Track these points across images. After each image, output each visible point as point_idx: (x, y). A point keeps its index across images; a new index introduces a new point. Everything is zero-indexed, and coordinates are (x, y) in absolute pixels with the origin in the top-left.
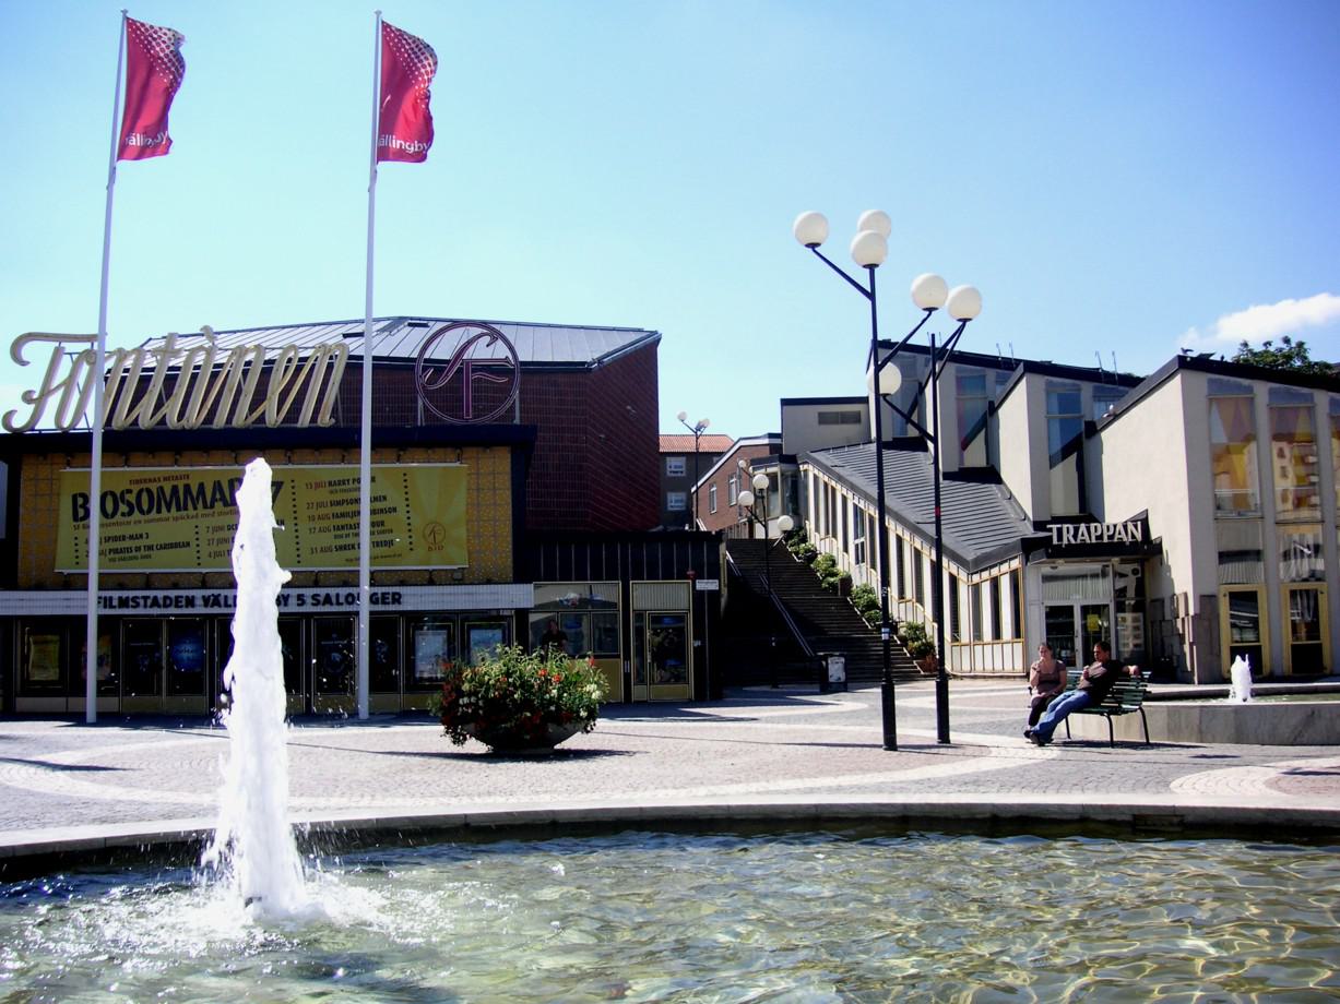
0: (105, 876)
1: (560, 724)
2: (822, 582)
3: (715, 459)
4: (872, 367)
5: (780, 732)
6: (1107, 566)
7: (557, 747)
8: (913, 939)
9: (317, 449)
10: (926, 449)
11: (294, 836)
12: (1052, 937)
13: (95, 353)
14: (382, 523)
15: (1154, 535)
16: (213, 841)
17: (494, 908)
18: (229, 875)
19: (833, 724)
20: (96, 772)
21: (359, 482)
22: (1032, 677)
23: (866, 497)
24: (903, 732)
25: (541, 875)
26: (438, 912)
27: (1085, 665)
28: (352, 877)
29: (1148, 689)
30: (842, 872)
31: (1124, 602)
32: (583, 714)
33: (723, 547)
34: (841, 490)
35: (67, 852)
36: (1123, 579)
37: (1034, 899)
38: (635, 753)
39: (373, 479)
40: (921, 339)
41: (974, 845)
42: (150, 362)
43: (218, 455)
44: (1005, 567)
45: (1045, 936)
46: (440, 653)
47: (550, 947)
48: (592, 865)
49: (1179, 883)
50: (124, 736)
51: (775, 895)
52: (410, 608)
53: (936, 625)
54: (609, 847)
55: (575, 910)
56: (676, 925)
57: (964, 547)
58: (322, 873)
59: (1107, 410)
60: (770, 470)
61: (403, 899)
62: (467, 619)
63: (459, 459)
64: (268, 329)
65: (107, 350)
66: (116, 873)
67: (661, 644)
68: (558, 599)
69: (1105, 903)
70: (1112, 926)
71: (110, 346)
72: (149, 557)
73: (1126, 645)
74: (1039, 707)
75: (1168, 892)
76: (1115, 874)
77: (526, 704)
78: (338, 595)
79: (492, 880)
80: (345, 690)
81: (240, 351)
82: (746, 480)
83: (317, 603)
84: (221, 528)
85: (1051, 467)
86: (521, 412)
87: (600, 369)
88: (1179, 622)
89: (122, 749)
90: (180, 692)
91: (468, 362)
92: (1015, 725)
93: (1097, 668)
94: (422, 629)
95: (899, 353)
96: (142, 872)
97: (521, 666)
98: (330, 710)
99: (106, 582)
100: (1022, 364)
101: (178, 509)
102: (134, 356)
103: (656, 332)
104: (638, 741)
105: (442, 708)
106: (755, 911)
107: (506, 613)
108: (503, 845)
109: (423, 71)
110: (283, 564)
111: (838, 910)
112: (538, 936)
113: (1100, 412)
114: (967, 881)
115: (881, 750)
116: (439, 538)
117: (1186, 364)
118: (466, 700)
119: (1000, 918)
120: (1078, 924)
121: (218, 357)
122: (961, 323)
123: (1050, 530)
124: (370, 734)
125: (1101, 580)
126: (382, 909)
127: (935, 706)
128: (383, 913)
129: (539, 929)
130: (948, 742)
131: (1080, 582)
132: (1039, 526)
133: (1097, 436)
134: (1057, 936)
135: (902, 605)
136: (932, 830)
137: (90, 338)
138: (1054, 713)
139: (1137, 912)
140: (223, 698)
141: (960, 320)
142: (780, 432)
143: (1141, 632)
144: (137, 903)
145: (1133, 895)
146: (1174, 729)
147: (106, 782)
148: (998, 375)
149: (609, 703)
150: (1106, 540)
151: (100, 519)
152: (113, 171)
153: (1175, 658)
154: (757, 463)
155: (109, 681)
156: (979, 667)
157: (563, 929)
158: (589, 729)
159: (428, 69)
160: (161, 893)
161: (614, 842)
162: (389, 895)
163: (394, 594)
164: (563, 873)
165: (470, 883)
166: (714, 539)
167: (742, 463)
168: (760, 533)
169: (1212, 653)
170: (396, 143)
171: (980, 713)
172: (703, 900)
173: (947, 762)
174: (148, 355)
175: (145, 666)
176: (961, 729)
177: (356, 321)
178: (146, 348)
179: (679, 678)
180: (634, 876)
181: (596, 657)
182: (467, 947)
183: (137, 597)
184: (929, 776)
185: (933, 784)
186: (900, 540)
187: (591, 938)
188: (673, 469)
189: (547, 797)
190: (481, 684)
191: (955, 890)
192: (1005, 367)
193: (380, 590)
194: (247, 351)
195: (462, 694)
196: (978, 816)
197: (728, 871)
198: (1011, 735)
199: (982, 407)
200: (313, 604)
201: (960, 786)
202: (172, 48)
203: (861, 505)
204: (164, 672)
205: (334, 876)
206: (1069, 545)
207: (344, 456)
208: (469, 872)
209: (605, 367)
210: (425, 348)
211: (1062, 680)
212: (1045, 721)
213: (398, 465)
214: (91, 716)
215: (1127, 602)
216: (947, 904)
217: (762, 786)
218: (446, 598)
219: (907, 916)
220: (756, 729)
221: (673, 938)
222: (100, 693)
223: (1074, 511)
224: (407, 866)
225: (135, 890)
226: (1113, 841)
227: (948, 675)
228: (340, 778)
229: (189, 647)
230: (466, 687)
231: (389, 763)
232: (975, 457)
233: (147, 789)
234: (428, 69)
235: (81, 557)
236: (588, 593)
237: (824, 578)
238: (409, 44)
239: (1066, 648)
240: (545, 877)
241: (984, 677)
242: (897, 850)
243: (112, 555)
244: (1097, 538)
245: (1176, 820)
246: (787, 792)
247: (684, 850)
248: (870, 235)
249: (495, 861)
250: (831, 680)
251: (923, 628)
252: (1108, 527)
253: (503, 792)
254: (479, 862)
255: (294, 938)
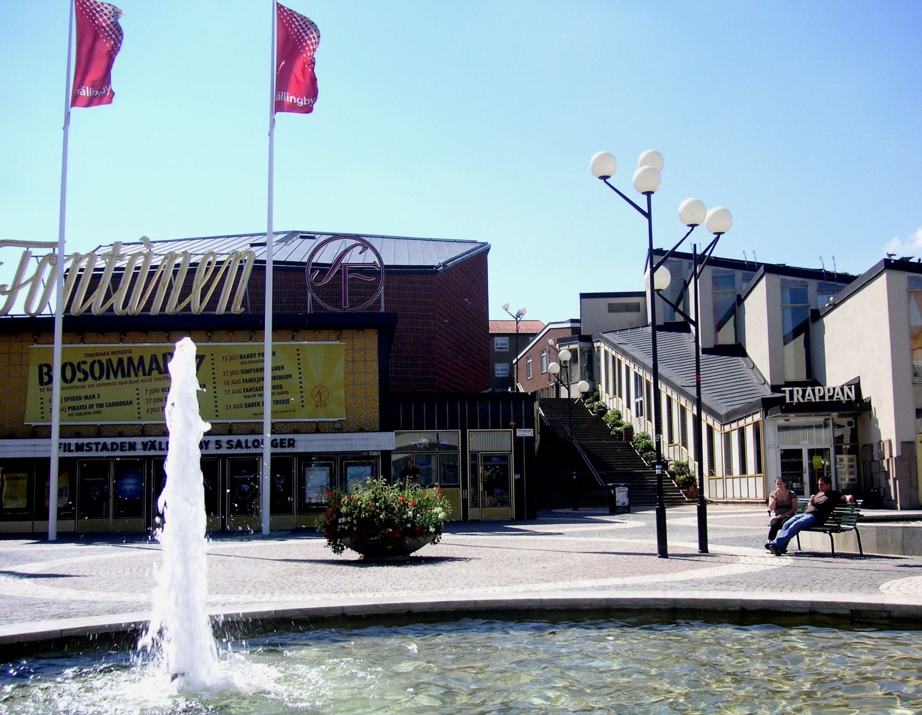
0: (60, 660)
1: (414, 537)
2: (611, 430)
3: (531, 338)
4: (649, 270)
5: (580, 543)
6: (829, 419)
7: (412, 555)
8: (682, 704)
9: (231, 331)
10: (689, 331)
11: (211, 625)
12: (790, 704)
13: (56, 256)
14: (281, 387)
15: (865, 396)
16: (147, 630)
17: (364, 678)
18: (159, 656)
19: (619, 537)
20: (55, 579)
21: (263, 356)
22: (770, 503)
23: (644, 367)
24: (673, 544)
25: (400, 652)
26: (321, 682)
27: (811, 494)
28: (255, 656)
29: (861, 513)
30: (628, 650)
31: (842, 446)
32: (432, 530)
33: (536, 405)
34: (625, 362)
35: (29, 642)
36: (841, 429)
37: (775, 674)
38: (470, 559)
39: (274, 354)
40: (686, 248)
41: (727, 630)
42: (100, 263)
43: (154, 335)
44: (749, 420)
45: (784, 703)
46: (325, 484)
47: (406, 709)
48: (438, 645)
49: (889, 664)
50: (79, 550)
51: (576, 668)
52: (301, 450)
53: (697, 463)
54: (451, 631)
55: (425, 680)
56: (501, 691)
57: (718, 404)
58: (232, 654)
59: (828, 301)
60: (572, 347)
61: (295, 672)
62: (345, 459)
63: (338, 338)
64: (192, 239)
65: (65, 254)
66: (69, 657)
67: (490, 477)
68: (413, 443)
69: (831, 678)
70: (836, 696)
71: (69, 250)
72: (100, 412)
73: (843, 479)
74: (776, 526)
75: (880, 671)
76: (838, 656)
77: (389, 522)
78: (247, 441)
79: (362, 657)
80: (252, 512)
81: (171, 256)
82: (553, 354)
83: (231, 447)
84: (157, 391)
85: (785, 344)
86: (385, 303)
87: (444, 271)
88: (885, 462)
89: (76, 560)
90: (125, 515)
91: (345, 265)
92: (758, 539)
93: (820, 497)
94: (311, 466)
95: (669, 258)
96: (91, 656)
97: (385, 494)
98: (240, 528)
99: (65, 432)
100: (763, 266)
101: (123, 376)
102: (87, 259)
103: (486, 243)
104: (473, 550)
105: (326, 526)
106: (561, 680)
107: (374, 454)
108: (371, 629)
109: (309, 42)
110: (205, 418)
111: (624, 680)
112: (397, 700)
113: (823, 302)
114: (722, 658)
115: (656, 557)
116: (324, 397)
117: (890, 265)
118: (343, 519)
119: (749, 688)
120: (810, 694)
121: (153, 260)
122: (716, 236)
123: (784, 392)
124: (271, 546)
125: (823, 430)
126: (278, 681)
127: (696, 524)
128: (279, 683)
129: (399, 694)
130: (707, 552)
131: (807, 431)
132: (775, 388)
133: (820, 321)
134: (793, 703)
135: (671, 448)
136: (694, 619)
137: (52, 245)
138: (787, 531)
139: (855, 686)
140: (158, 520)
141: (715, 233)
142: (579, 318)
143: (855, 470)
144: (86, 681)
145: (853, 673)
146: (881, 544)
147: (64, 586)
148: (744, 275)
149: (451, 522)
150: (827, 399)
151: (61, 385)
152: (68, 115)
153: (882, 490)
154: (562, 341)
155: (68, 507)
156: (730, 495)
157: (416, 694)
158: (436, 541)
159: (313, 41)
160: (105, 672)
161: (455, 627)
162: (283, 669)
163: (290, 440)
164: (416, 651)
165: (345, 660)
166: (530, 398)
167: (551, 342)
168: (564, 394)
169: (911, 486)
170: (289, 99)
171: (731, 530)
172: (522, 672)
173: (706, 567)
174: (99, 259)
175: (96, 496)
176: (717, 542)
177: (260, 234)
178: (97, 253)
179: (504, 503)
180: (470, 653)
181: (441, 487)
182: (342, 709)
183: (90, 443)
184: (693, 578)
185: (696, 584)
186: (669, 399)
187: (436, 701)
188: (499, 346)
189: (404, 593)
190: (355, 507)
191: (714, 666)
192: (750, 268)
193: (278, 437)
194: (177, 256)
195: (340, 515)
196: (730, 609)
197: (541, 649)
198: (755, 547)
199: (732, 299)
200: (228, 448)
201: (716, 585)
202: (112, 20)
203: (640, 373)
204: (111, 500)
205: (241, 656)
206: (799, 403)
207: (251, 336)
208: (345, 650)
209: (448, 269)
210: (313, 255)
211: (793, 506)
212: (781, 537)
213: (293, 343)
214: (52, 535)
215: (844, 447)
216: (708, 676)
217: (566, 584)
218: (328, 443)
219: (677, 685)
220: (561, 541)
221: (500, 701)
222: (60, 517)
223: (803, 377)
224: (297, 647)
225: (85, 670)
226: (836, 630)
227: (706, 501)
228: (247, 580)
229: (131, 481)
230: (344, 510)
231: (284, 568)
232: (727, 337)
233: (96, 590)
234: (313, 41)
235: (46, 412)
236: (435, 438)
237: (612, 428)
238: (298, 21)
239: (797, 481)
240: (403, 654)
241: (734, 503)
242: (669, 634)
243: (71, 411)
244: (820, 398)
245: (885, 615)
246: (585, 589)
247: (507, 633)
248: (647, 170)
249: (365, 642)
250: (618, 504)
251: (687, 466)
252: (829, 389)
253: (371, 589)
254: (353, 643)
255: (209, 705)
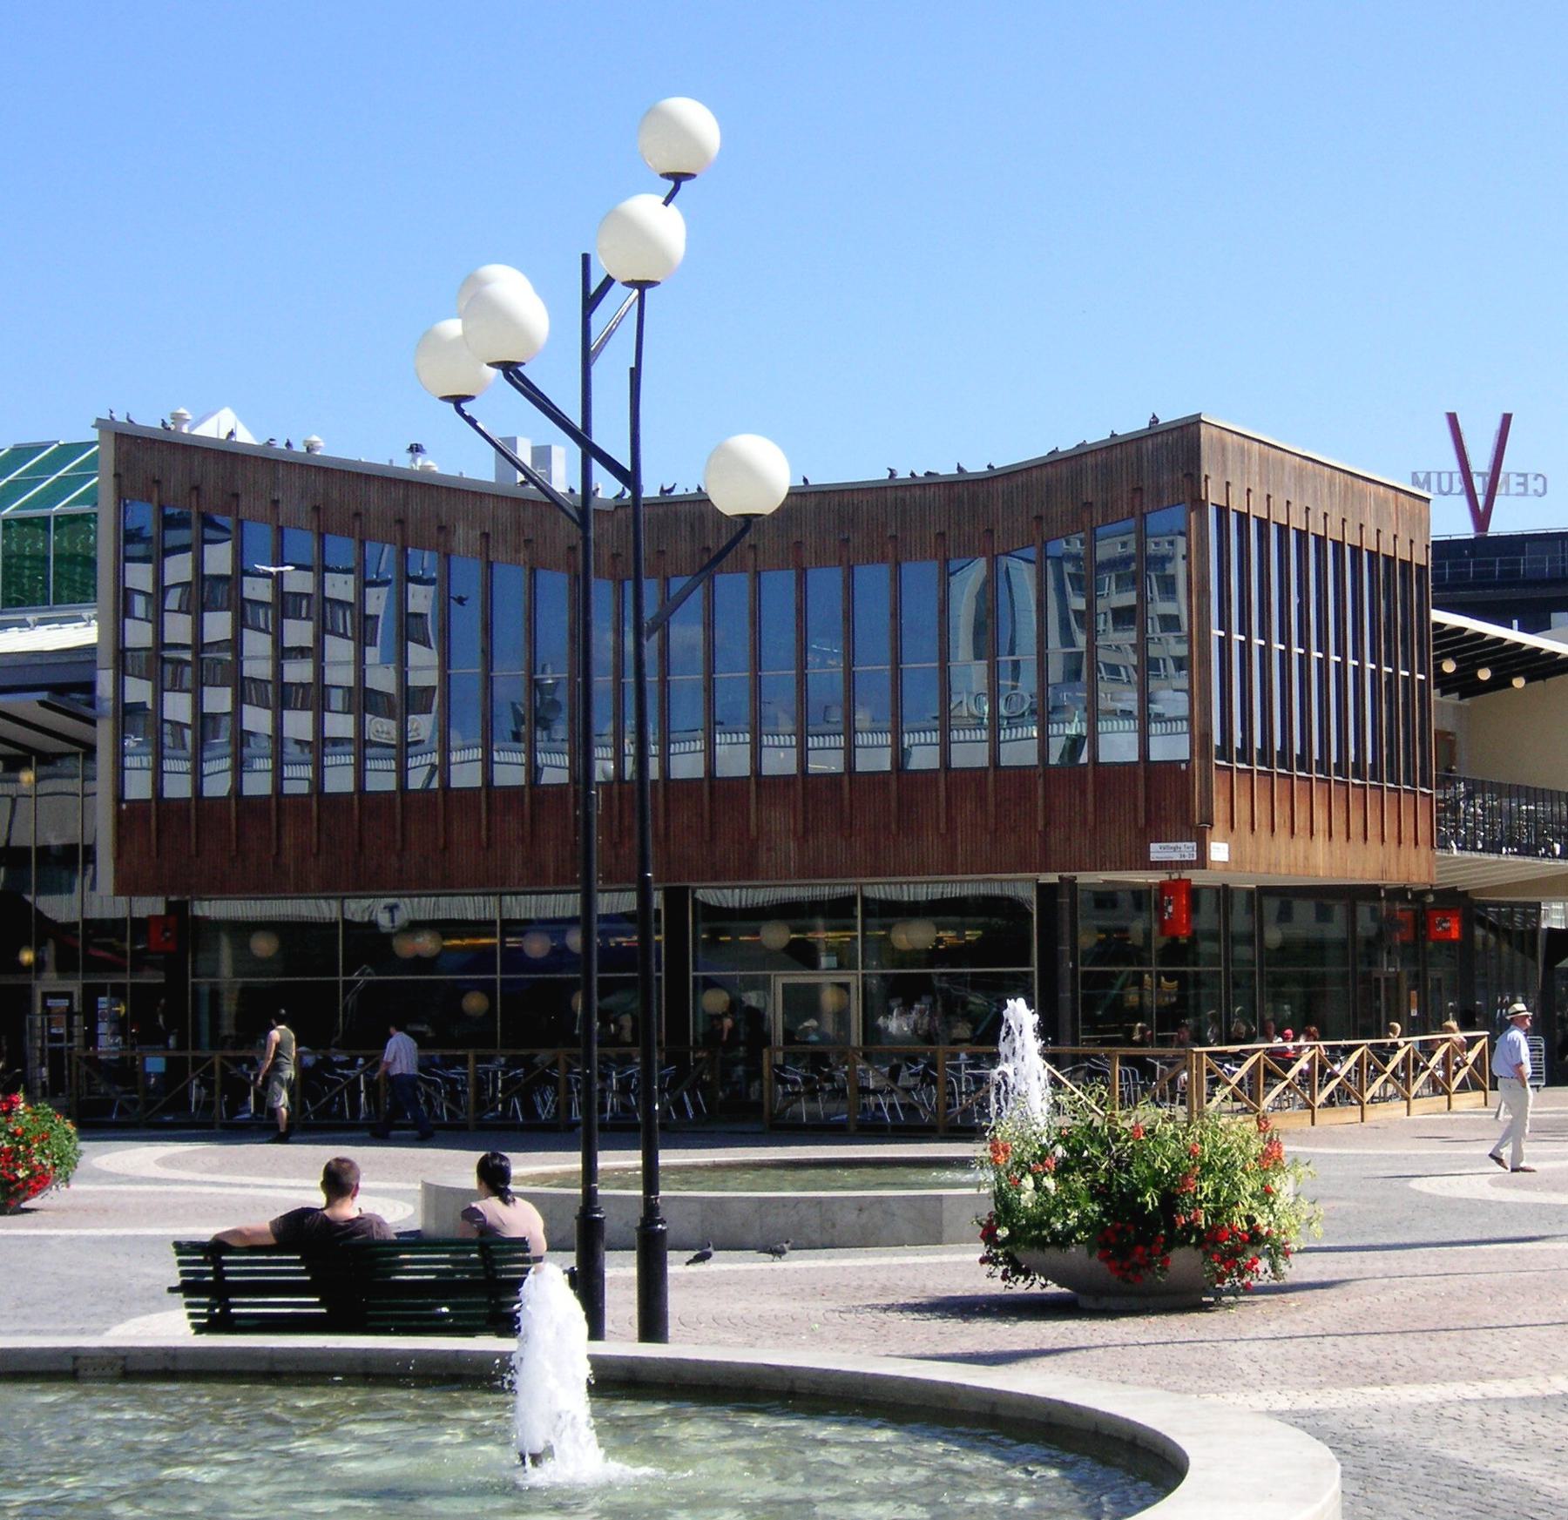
141: (668, 176)
